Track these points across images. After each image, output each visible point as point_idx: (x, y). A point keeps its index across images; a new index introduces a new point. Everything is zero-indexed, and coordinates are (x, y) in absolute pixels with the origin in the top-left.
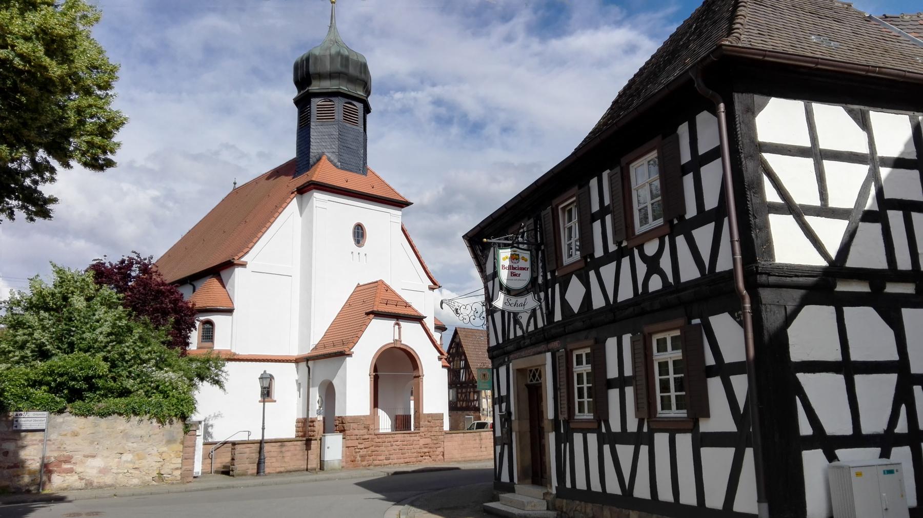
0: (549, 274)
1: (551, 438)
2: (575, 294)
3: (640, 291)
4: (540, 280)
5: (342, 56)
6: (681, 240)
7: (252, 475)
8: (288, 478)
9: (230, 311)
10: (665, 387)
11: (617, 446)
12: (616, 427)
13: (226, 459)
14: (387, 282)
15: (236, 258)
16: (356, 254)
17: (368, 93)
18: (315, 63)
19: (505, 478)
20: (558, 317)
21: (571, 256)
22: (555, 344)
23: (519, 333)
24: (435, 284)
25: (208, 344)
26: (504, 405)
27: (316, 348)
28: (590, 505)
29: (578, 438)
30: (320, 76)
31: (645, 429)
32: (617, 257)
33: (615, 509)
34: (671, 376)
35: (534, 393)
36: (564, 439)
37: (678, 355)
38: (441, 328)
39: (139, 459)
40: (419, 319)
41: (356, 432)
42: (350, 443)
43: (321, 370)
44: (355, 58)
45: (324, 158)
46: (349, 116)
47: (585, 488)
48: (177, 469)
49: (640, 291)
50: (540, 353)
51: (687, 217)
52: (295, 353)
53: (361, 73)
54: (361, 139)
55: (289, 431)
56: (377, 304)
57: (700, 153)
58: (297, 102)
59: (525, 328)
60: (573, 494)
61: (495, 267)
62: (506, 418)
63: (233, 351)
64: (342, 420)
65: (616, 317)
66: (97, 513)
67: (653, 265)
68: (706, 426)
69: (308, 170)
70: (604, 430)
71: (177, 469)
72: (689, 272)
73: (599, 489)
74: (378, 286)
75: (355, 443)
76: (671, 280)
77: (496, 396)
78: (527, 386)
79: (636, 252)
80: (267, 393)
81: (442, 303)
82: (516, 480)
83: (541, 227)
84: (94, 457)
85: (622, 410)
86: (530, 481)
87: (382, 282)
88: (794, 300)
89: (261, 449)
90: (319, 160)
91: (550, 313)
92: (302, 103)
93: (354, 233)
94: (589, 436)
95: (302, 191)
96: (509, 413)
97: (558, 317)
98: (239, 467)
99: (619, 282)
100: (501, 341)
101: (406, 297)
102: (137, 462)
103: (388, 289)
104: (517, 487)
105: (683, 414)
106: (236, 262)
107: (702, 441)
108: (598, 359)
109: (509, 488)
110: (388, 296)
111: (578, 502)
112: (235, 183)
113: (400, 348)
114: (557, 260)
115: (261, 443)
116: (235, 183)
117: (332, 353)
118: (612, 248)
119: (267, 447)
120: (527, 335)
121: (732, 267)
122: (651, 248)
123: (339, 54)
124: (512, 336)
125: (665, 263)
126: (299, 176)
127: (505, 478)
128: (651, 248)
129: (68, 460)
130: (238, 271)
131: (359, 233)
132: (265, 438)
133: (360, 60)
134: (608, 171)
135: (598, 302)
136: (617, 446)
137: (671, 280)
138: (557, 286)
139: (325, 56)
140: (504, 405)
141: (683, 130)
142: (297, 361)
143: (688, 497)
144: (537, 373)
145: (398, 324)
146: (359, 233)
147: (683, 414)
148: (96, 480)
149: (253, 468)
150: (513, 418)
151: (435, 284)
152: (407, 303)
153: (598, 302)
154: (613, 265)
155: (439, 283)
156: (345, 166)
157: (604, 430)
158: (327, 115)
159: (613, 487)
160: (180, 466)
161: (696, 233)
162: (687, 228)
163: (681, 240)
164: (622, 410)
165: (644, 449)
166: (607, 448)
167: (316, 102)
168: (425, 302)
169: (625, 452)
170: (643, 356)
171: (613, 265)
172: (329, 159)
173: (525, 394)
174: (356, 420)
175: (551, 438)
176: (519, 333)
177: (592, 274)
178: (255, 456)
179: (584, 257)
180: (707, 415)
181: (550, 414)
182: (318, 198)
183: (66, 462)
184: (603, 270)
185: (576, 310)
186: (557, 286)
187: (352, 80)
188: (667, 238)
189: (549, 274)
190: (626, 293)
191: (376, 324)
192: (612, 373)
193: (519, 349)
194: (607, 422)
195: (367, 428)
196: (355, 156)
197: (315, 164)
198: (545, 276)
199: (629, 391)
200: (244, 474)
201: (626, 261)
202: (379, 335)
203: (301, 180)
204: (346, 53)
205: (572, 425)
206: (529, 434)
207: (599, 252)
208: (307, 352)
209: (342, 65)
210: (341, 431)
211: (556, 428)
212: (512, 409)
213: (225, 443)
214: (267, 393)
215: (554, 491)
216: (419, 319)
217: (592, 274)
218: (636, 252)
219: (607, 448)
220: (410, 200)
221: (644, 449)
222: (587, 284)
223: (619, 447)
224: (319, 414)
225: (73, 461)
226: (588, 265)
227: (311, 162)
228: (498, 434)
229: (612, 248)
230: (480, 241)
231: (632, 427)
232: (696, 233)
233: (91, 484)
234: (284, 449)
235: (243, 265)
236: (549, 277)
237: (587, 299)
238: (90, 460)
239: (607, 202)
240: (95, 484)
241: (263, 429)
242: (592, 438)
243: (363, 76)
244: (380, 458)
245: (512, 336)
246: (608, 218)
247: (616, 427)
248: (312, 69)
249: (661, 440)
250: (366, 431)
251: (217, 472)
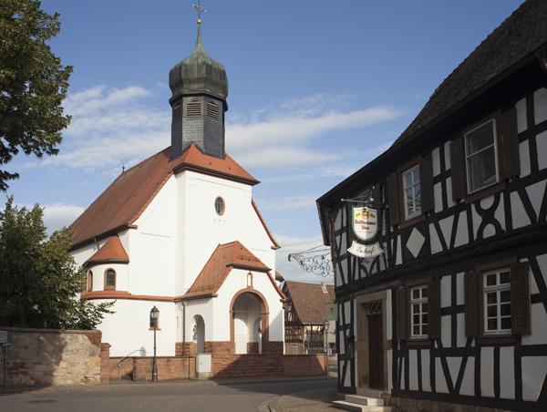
0: (391, 228)
1: (389, 355)
2: (415, 242)
3: (475, 237)
4: (384, 233)
5: (207, 65)
6: (515, 196)
7: (149, 380)
8: (173, 384)
9: (126, 262)
10: (492, 312)
11: (448, 358)
12: (447, 343)
13: (129, 369)
16: (217, 220)
17: (226, 95)
18: (186, 71)
19: (347, 383)
20: (399, 261)
21: (412, 212)
22: (394, 283)
23: (363, 275)
24: (276, 245)
25: (111, 287)
26: (348, 331)
27: (188, 292)
28: (421, 401)
29: (413, 354)
30: (191, 81)
31: (473, 345)
32: (455, 212)
33: (442, 403)
34: (499, 303)
35: (375, 322)
36: (401, 354)
37: (507, 286)
38: (280, 279)
40: (266, 270)
42: (217, 361)
44: (216, 66)
45: (193, 145)
47: (417, 389)
49: (475, 237)
50: (383, 290)
51: (436, 211)
52: (174, 295)
53: (221, 78)
54: (221, 131)
56: (234, 257)
57: (537, 123)
59: (368, 271)
60: (408, 393)
61: (347, 222)
62: (350, 340)
65: (452, 260)
66: (52, 401)
67: (488, 216)
68: (526, 341)
70: (436, 346)
72: (521, 220)
73: (429, 390)
74: (236, 245)
75: (220, 361)
76: (504, 227)
77: (341, 324)
78: (368, 316)
79: (473, 207)
80: (154, 324)
81: (290, 256)
82: (357, 385)
83: (386, 190)
84: (40, 364)
85: (451, 331)
86: (367, 386)
87: (238, 242)
89: (154, 363)
90: (189, 147)
91: (392, 258)
92: (176, 102)
93: (216, 204)
94: (423, 351)
95: (177, 171)
96: (352, 337)
97: (399, 261)
98: (139, 374)
99: (457, 232)
100: (346, 282)
101: (256, 254)
103: (242, 247)
104: (358, 390)
105: (507, 332)
107: (521, 352)
108: (434, 293)
109: (352, 390)
110: (243, 253)
111: (410, 400)
113: (252, 293)
114: (400, 216)
117: (202, 293)
118: (451, 204)
120: (370, 276)
121: (228, 339)
122: (486, 204)
123: (204, 63)
124: (357, 278)
125: (500, 215)
126: (175, 160)
127: (347, 383)
128: (486, 204)
129: (22, 365)
130: (131, 231)
131: (220, 205)
133: (221, 68)
134: (450, 142)
135: (436, 247)
136: (448, 358)
137: (504, 227)
138: (399, 237)
140: (348, 331)
141: (521, 106)
142: (176, 300)
143: (508, 392)
144: (379, 305)
146: (220, 205)
147: (507, 332)
149: (149, 377)
150: (356, 340)
151: (276, 245)
153: (436, 247)
154: (452, 218)
157: (436, 346)
159: (442, 387)
161: (529, 189)
162: (521, 185)
163: (515, 196)
164: (451, 331)
165: (471, 360)
166: (438, 360)
167: (187, 101)
168: (268, 258)
169: (454, 363)
170: (473, 290)
171: (452, 218)
172: (197, 146)
173: (365, 322)
174: (220, 344)
175: (389, 355)
176: (363, 275)
177: (432, 227)
178: (150, 367)
179: (425, 213)
180: (529, 333)
181: (389, 335)
183: (22, 367)
184: (442, 223)
185: (416, 256)
186: (399, 237)
187: (214, 84)
188: (502, 195)
189: (391, 228)
190: (462, 239)
192: (446, 301)
193: (363, 288)
194: (439, 341)
195: (229, 350)
196: (214, 143)
197: (185, 151)
198: (388, 229)
199: (461, 317)
200: (143, 380)
201: (463, 215)
202: (236, 281)
203: (176, 163)
204: (210, 63)
205: (408, 344)
206: (368, 352)
207: (439, 208)
208: (182, 294)
209: (207, 73)
210: (209, 352)
211: (394, 348)
212: (355, 334)
213: (127, 358)
214: (154, 324)
215: (390, 392)
216: (266, 270)
217: (432, 227)
218: (473, 207)
219: (438, 360)
220: (259, 180)
221: (471, 360)
222: (426, 235)
223: (449, 360)
224: (194, 339)
226: (429, 218)
228: (342, 351)
229: (451, 204)
230: (333, 205)
231: (461, 343)
232: (529, 189)
233: (39, 382)
234: (170, 363)
235: (135, 228)
236: (392, 230)
237: (427, 245)
238: (37, 366)
239: (448, 167)
240: (42, 382)
241: (155, 348)
242: (426, 354)
243: (222, 81)
245: (357, 278)
246: (449, 181)
247: (447, 343)
248: (183, 76)
249: (487, 353)
250: (227, 352)
251: (122, 378)
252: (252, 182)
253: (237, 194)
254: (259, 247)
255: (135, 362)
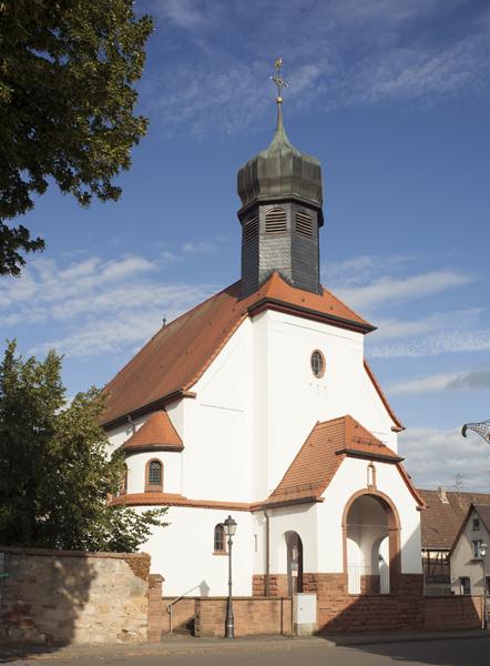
5: (294, 157)
7: (219, 636)
9: (179, 449)
14: (356, 417)
15: (185, 388)
25: (155, 488)
27: (273, 495)
30: (270, 182)
39: (103, 612)
41: (329, 592)
43: (284, 522)
45: (276, 274)
46: (301, 226)
48: (142, 626)
52: (251, 500)
53: (315, 178)
55: (244, 588)
58: (242, 216)
63: (183, 495)
64: (314, 578)
69: (258, 290)
71: (142, 626)
74: (346, 423)
87: (350, 418)
88: (97, 586)
89: (228, 607)
92: (248, 215)
95: (254, 312)
102: (100, 615)
103: (357, 426)
106: (184, 393)
110: (359, 433)
112: (164, 320)
113: (373, 496)
115: (228, 599)
116: (164, 320)
119: (235, 605)
126: (249, 295)
129: (26, 610)
131: (317, 362)
132: (233, 595)
139: (275, 159)
142: (253, 509)
145: (371, 466)
146: (317, 362)
148: (55, 635)
149: (220, 630)
152: (381, 442)
155: (402, 425)
156: (298, 284)
158: (276, 224)
160: (145, 622)
174: (329, 577)
178: (222, 615)
182: (271, 315)
191: (348, 463)
196: (306, 271)
197: (264, 283)
200: (211, 634)
202: (351, 478)
203: (253, 299)
208: (264, 497)
216: (395, 461)
225: (31, 611)
227: (260, 280)
234: (252, 608)
235: (193, 396)
238: (49, 611)
240: (55, 639)
241: (230, 584)
244: (356, 623)
251: (176, 631)
252: (364, 329)
253: (344, 348)
254: (377, 424)
255: (197, 606)
